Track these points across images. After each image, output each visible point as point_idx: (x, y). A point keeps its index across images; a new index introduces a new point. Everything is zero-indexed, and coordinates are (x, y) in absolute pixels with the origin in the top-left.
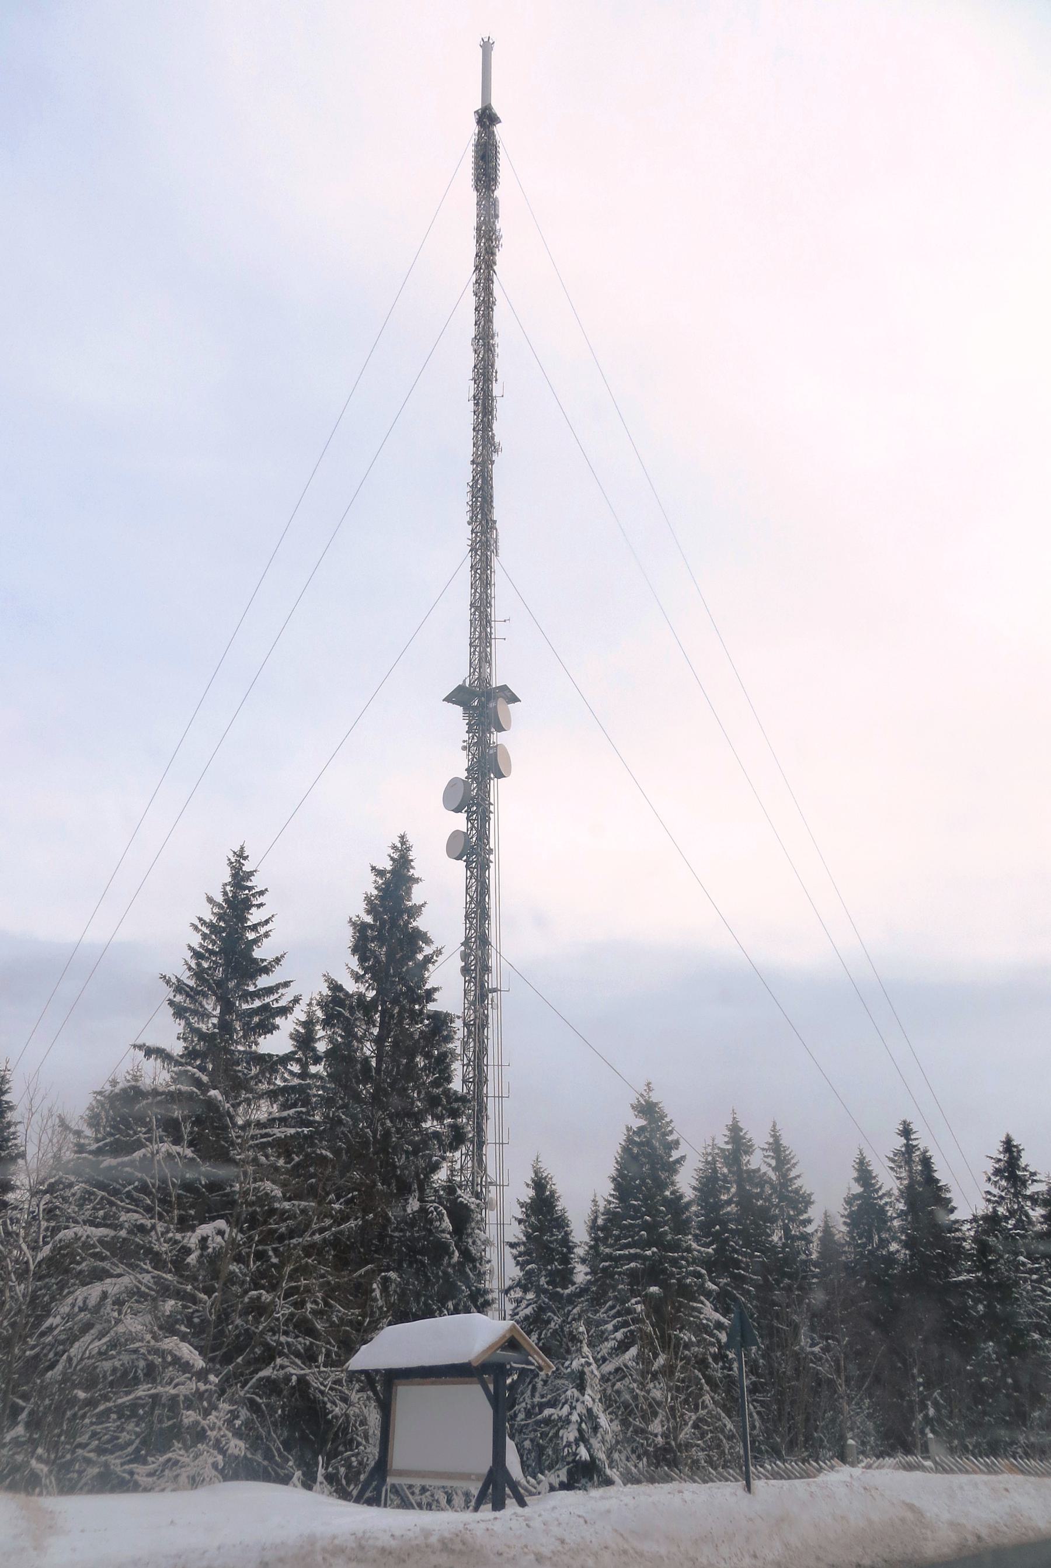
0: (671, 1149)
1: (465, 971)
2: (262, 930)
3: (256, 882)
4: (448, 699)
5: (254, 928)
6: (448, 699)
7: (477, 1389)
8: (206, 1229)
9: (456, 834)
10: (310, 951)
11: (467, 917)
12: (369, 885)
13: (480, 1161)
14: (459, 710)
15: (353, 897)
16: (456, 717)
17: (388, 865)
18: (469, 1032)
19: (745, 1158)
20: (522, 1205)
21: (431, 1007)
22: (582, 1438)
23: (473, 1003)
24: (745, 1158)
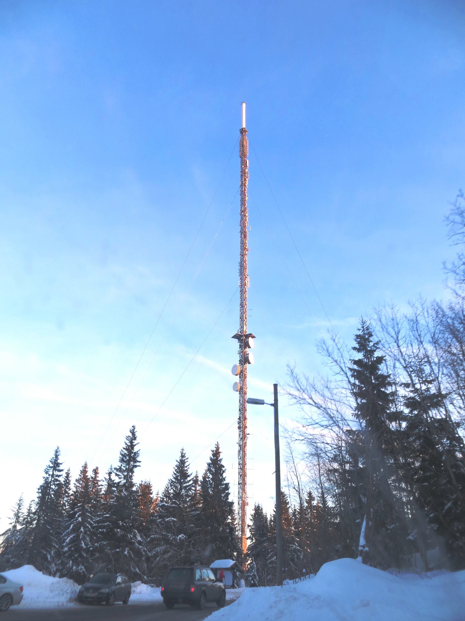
0: (388, 401)
1: (239, 428)
2: (188, 467)
3: (187, 456)
4: (233, 337)
5: (186, 467)
6: (233, 337)
7: (230, 572)
8: (180, 536)
9: (236, 383)
10: (198, 468)
11: (240, 410)
12: (210, 454)
13: (244, 490)
14: (237, 340)
15: (207, 457)
16: (236, 343)
17: (215, 449)
18: (241, 448)
19: (313, 502)
20: (252, 515)
21: (225, 482)
22: (252, 579)
23: (242, 439)
24: (313, 502)
